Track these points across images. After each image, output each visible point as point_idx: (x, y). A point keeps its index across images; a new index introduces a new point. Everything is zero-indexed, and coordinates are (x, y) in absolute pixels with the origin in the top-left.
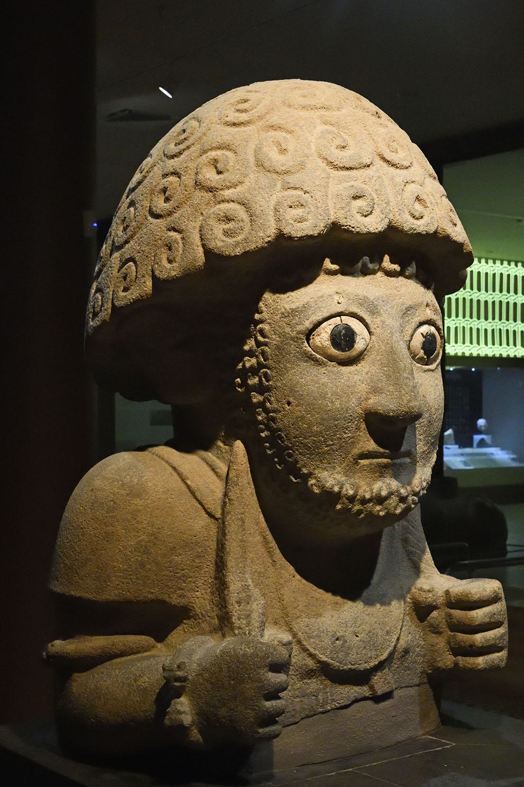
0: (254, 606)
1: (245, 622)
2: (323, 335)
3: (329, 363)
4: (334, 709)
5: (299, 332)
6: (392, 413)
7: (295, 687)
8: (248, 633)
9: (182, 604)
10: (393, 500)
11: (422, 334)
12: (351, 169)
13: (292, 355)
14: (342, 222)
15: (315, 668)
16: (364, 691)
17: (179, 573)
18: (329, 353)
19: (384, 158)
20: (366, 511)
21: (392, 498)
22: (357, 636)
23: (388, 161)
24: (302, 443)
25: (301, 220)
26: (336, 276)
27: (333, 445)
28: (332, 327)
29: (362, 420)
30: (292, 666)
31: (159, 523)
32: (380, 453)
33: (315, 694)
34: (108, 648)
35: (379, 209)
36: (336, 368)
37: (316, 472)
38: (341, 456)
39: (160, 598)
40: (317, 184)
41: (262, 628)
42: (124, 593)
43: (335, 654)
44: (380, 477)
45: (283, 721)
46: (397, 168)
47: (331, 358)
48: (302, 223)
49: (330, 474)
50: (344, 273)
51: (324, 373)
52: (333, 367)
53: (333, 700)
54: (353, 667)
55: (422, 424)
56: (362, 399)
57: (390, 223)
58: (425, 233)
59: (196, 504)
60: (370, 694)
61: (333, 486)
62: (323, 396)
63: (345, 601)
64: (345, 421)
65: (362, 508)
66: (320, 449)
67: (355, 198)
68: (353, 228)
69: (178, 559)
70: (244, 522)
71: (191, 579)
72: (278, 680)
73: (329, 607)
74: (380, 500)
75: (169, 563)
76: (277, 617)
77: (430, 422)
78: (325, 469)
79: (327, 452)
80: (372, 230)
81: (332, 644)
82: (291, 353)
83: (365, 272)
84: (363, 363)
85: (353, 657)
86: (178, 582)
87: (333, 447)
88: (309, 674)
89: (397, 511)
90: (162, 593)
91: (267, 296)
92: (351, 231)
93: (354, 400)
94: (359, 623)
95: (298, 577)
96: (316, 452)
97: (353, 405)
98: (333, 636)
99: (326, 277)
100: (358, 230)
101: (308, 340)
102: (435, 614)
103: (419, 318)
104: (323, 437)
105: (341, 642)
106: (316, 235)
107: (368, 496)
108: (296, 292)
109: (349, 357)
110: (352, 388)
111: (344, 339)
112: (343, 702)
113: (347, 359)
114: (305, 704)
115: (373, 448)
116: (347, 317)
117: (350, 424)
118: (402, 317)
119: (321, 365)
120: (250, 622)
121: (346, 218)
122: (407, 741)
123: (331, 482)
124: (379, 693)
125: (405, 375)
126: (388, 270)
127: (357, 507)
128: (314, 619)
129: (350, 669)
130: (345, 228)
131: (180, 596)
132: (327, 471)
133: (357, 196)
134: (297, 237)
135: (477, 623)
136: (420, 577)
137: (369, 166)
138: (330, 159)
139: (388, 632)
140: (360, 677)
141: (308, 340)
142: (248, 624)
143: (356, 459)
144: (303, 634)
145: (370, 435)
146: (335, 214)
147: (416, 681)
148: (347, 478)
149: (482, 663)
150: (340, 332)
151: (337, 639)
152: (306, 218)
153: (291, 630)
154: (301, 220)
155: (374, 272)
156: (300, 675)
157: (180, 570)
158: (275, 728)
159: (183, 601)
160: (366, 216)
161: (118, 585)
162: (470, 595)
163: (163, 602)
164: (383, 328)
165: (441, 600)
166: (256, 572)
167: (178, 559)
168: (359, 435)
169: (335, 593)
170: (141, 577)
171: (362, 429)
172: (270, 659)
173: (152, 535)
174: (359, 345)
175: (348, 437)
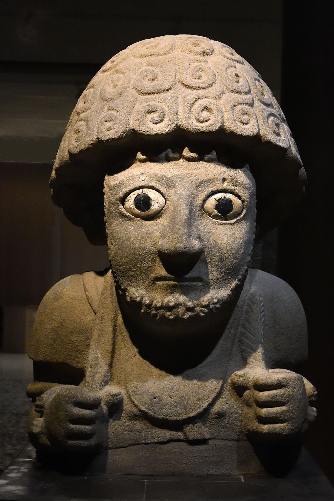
0: (100, 370)
1: (91, 379)
2: (130, 201)
3: (136, 218)
4: (153, 443)
5: (116, 200)
6: (166, 251)
7: (126, 424)
8: (91, 386)
9: (79, 367)
10: (181, 310)
11: (215, 199)
12: (153, 94)
13: (113, 214)
14: (137, 128)
15: (138, 414)
16: (179, 435)
17: (76, 348)
18: (134, 212)
19: (184, 83)
20: (160, 315)
21: (181, 308)
22: (172, 398)
23: (187, 86)
24: (119, 269)
25: (109, 129)
26: (145, 163)
27: (135, 271)
28: (135, 196)
29: (157, 256)
30: (124, 411)
31: (64, 316)
32: (169, 277)
33: (139, 431)
34: (43, 389)
35: (168, 118)
36: (140, 222)
37: (128, 288)
38: (143, 278)
39: (66, 362)
40: (126, 105)
41: (102, 384)
42: (46, 356)
43: (152, 407)
44: (171, 293)
45: (115, 444)
46: (194, 89)
47: (137, 216)
48: (110, 131)
49: (136, 289)
50: (152, 161)
51: (132, 225)
52: (138, 221)
53: (153, 437)
54: (165, 417)
55: (214, 260)
56: (156, 242)
57: (177, 125)
58: (208, 131)
59: (89, 307)
60: (185, 438)
61: (137, 297)
62: (128, 239)
63: (168, 374)
64: (143, 256)
65: (157, 313)
66: (128, 273)
67: (150, 112)
68: (144, 132)
69: (75, 339)
70: (102, 318)
71: (83, 352)
72: (81, 413)
73: (154, 377)
74: (170, 308)
75: (69, 341)
76: (120, 380)
77: (221, 259)
78: (133, 286)
79: (133, 276)
80: (160, 132)
81: (150, 400)
82: (113, 213)
83: (168, 160)
84: (161, 219)
85: (165, 411)
86: (76, 353)
87: (136, 272)
88: (134, 417)
89: (185, 317)
90: (66, 359)
91: (107, 177)
92: (143, 134)
93: (149, 242)
94: (175, 389)
95: (138, 356)
96: (127, 275)
97: (149, 246)
98: (152, 395)
99: (139, 164)
100: (148, 133)
101: (123, 205)
102: (247, 392)
103: (212, 189)
104: (129, 266)
105: (158, 400)
106: (116, 138)
107: (159, 305)
108: (118, 174)
109: (148, 215)
110: (156, 235)
111: (143, 203)
112: (160, 440)
113: (147, 216)
114: (131, 436)
115: (164, 274)
116: (147, 189)
117: (147, 258)
118: (196, 188)
119: (130, 220)
120: (93, 379)
121: (139, 126)
122: (220, 475)
123: (136, 295)
124: (191, 438)
125: (178, 226)
126: (187, 157)
127: (154, 312)
128: (141, 383)
129: (163, 418)
130: (139, 132)
131: (77, 362)
132: (135, 287)
133: (151, 111)
134: (105, 140)
135: (262, 400)
136: (246, 367)
137: (167, 90)
138: (138, 89)
139: (199, 399)
140: (178, 426)
141: (123, 205)
142: (92, 380)
143: (153, 281)
144: (132, 391)
145: (163, 265)
146: (133, 124)
147: (234, 436)
148: (147, 293)
149: (266, 429)
150: (141, 198)
151: (155, 398)
152: (112, 128)
153: (126, 388)
154: (109, 129)
155: (176, 159)
156: (129, 417)
157: (76, 346)
158: (81, 442)
159: (80, 366)
160: (156, 123)
161: (43, 351)
162: (258, 381)
163: (67, 364)
164: (175, 195)
165: (250, 384)
166: (105, 349)
167: (75, 339)
168: (155, 266)
169: (161, 369)
170: (54, 348)
171: (157, 262)
172: (75, 399)
173: (60, 323)
174: (155, 207)
175: (147, 266)
